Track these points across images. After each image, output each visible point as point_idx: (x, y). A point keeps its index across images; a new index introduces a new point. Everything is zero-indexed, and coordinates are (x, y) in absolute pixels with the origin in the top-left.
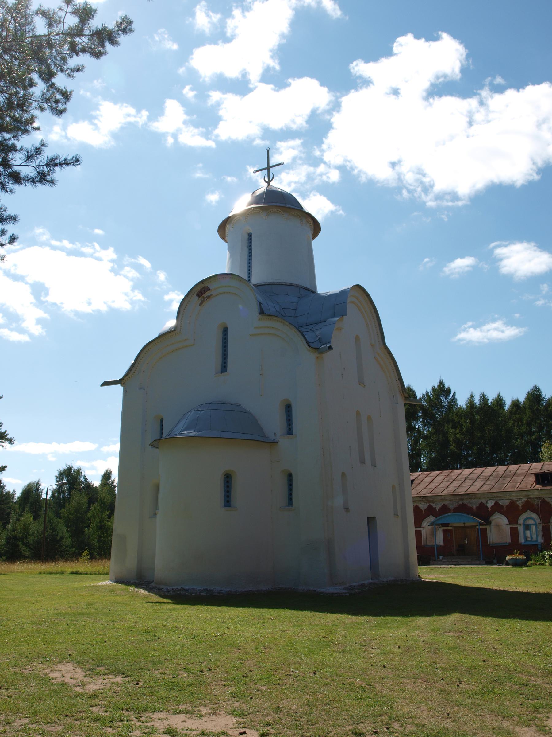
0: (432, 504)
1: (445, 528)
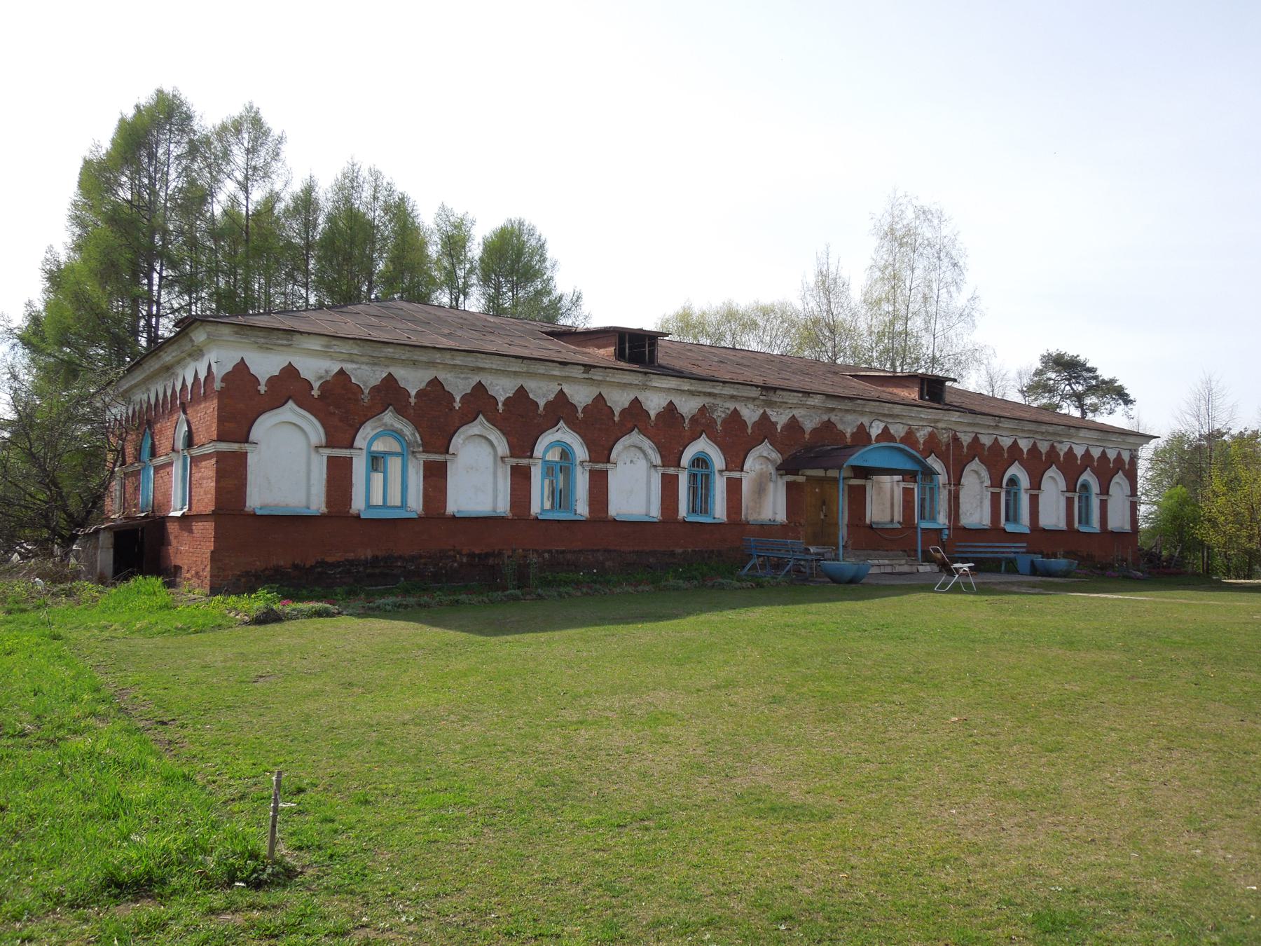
0: (769, 412)
1: (790, 478)
